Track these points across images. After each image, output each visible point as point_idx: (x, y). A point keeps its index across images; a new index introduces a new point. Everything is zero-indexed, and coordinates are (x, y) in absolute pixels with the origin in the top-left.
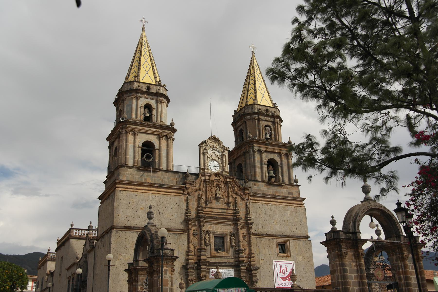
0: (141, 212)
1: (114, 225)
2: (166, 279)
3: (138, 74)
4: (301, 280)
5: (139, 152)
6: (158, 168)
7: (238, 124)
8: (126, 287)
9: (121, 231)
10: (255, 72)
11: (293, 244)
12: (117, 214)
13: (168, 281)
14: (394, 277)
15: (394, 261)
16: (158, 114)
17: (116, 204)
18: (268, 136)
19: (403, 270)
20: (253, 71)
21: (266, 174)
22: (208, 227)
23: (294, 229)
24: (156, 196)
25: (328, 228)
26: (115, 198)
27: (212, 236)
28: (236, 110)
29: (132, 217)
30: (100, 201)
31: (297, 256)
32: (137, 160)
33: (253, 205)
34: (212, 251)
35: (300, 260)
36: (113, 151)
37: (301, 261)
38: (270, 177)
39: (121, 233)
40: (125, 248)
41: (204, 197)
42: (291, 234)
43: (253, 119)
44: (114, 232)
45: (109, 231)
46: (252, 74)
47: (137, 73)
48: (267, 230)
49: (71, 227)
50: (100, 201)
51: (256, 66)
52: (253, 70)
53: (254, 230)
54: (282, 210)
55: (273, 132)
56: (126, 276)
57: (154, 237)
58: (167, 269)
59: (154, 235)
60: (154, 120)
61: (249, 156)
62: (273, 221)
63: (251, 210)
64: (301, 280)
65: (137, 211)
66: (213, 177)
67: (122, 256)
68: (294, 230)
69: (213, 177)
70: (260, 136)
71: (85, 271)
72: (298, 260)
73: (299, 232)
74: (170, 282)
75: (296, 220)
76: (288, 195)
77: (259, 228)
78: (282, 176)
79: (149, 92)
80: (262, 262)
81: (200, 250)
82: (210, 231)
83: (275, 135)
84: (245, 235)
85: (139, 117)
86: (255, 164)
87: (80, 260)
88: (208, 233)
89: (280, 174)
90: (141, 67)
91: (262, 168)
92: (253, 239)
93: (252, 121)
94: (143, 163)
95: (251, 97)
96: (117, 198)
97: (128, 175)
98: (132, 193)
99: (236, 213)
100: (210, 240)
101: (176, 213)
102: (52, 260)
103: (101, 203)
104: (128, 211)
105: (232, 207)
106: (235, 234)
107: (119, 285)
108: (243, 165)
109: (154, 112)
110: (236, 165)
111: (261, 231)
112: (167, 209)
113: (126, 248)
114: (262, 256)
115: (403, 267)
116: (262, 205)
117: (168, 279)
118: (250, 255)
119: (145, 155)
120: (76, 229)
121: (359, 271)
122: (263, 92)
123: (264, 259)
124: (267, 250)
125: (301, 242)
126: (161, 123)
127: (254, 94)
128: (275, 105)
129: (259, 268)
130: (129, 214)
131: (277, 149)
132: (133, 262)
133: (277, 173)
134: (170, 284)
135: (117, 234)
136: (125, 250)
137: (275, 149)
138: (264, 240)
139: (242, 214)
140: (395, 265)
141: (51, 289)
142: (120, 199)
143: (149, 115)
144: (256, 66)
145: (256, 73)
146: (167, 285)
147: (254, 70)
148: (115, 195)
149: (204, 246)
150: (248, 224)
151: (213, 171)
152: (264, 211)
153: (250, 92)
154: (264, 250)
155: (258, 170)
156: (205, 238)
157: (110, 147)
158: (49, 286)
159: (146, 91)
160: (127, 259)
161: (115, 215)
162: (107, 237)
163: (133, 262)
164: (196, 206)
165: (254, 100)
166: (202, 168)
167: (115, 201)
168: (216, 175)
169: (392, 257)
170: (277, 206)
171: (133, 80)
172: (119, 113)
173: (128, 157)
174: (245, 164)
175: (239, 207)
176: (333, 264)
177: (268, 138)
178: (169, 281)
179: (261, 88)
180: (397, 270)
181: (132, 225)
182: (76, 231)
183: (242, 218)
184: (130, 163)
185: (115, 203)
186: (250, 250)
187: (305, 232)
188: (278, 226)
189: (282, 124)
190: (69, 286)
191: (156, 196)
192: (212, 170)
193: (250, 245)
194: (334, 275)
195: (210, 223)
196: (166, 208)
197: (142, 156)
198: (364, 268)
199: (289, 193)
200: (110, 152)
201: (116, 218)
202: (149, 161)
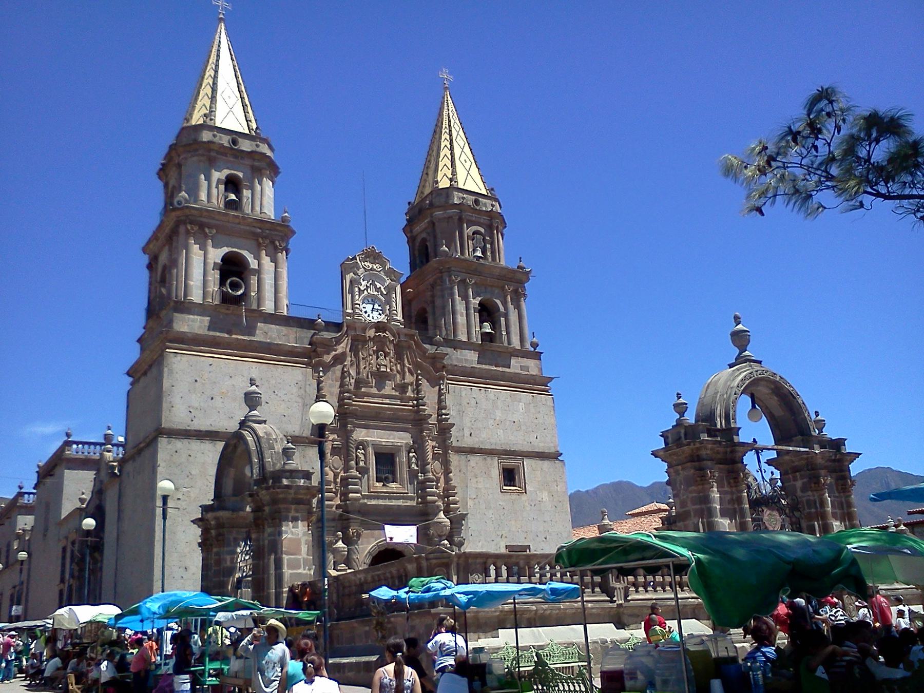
0: (221, 400)
1: (163, 426)
2: (297, 537)
3: (212, 111)
4: (546, 538)
5: (214, 276)
6: (256, 308)
7: (417, 229)
8: (920, 559)
9: (177, 440)
10: (452, 125)
11: (531, 469)
12: (171, 402)
13: (301, 542)
14: (800, 525)
15: (799, 490)
16: (256, 195)
17: (166, 384)
18: (479, 254)
19: (819, 510)
20: (447, 123)
21: (476, 329)
22: (363, 433)
23: (533, 439)
24: (254, 367)
25: (669, 421)
26: (166, 369)
27: (370, 450)
28: (412, 201)
29: (203, 411)
30: (131, 379)
31: (538, 492)
32: (211, 290)
33: (453, 390)
34: (371, 482)
35: (544, 500)
36: (157, 273)
37: (545, 502)
38: (485, 336)
39: (179, 444)
40: (188, 477)
41: (353, 372)
42: (527, 448)
43: (449, 217)
44: (163, 442)
45: (148, 445)
46: (213, 63)
47: (208, 108)
48: (481, 439)
49: (66, 438)
50: (161, 167)
51: (453, 114)
52: (447, 121)
53: (457, 437)
54: (509, 400)
55: (488, 246)
56: (196, 533)
57: (264, 445)
58: (297, 515)
59: (265, 440)
60: (248, 209)
61: (442, 291)
62: (491, 422)
63: (449, 400)
64: (546, 538)
65: (212, 399)
66: (371, 333)
67: (182, 493)
68: (531, 441)
69: (371, 333)
70: (462, 253)
71: (100, 525)
72: (540, 499)
73: (541, 445)
74: (306, 544)
75: (536, 421)
76: (520, 371)
77: (465, 435)
78: (508, 333)
79: (235, 149)
80: (470, 503)
81: (345, 482)
82: (366, 441)
83: (493, 253)
84: (436, 449)
85: (214, 201)
86: (454, 306)
87: (87, 505)
88: (363, 445)
89: (503, 328)
90: (219, 98)
91: (468, 315)
92: (454, 458)
93: (448, 222)
94: (226, 299)
95: (445, 174)
96: (169, 369)
97: (192, 321)
98: (203, 359)
99: (418, 405)
100: (368, 458)
101: (296, 404)
102: (28, 510)
103: (132, 384)
104: (193, 398)
105: (410, 393)
106: (418, 447)
107: (176, 554)
108: (429, 309)
109: (246, 193)
110: (413, 311)
111: (468, 442)
112: (277, 395)
113: (190, 477)
114: (472, 493)
115: (818, 505)
116: (470, 390)
117: (299, 539)
118: (448, 492)
119: (229, 281)
120: (77, 443)
121: (845, 506)
122: (467, 165)
123: (475, 497)
124: (480, 479)
125: (546, 464)
126: (262, 215)
127: (451, 169)
128: (492, 192)
129: (466, 514)
130: (196, 405)
131: (373, 476)
132: (212, 502)
133: (497, 326)
134: (306, 549)
135: (170, 447)
136: (188, 479)
137: (373, 473)
138: (475, 460)
139: (430, 408)
140: (799, 500)
141: (25, 567)
142: (175, 372)
143: (235, 198)
144: (453, 114)
145: (452, 127)
146: (298, 552)
147: (449, 121)
148: (165, 364)
149: (354, 472)
150: (444, 430)
151: (370, 318)
152: (473, 402)
153: (441, 165)
154: (474, 480)
155: (461, 320)
156: (357, 456)
157: (150, 267)
158: (20, 559)
159: (229, 146)
160: (192, 499)
161: (165, 405)
162: (146, 453)
163: (212, 502)
164: (337, 390)
165: (451, 180)
166: (348, 311)
167: (165, 375)
168: (379, 326)
169: (792, 483)
170: (498, 395)
171: (201, 122)
172: (170, 194)
173: (192, 283)
174: (434, 307)
175: (425, 393)
176: (685, 497)
177: (480, 257)
178: (303, 542)
179: (463, 157)
180: (804, 509)
181: (203, 428)
182: (78, 445)
183: (432, 415)
184: (196, 296)
185: (165, 381)
186: (448, 480)
187: (552, 445)
188: (500, 432)
189: (505, 231)
190: (64, 558)
191: (254, 367)
192: (369, 316)
193: (447, 472)
194: (687, 522)
195: (366, 427)
196: (274, 392)
197: (222, 283)
198: (718, 507)
199: (522, 368)
200: (150, 278)
201: (168, 412)
202: (234, 293)
